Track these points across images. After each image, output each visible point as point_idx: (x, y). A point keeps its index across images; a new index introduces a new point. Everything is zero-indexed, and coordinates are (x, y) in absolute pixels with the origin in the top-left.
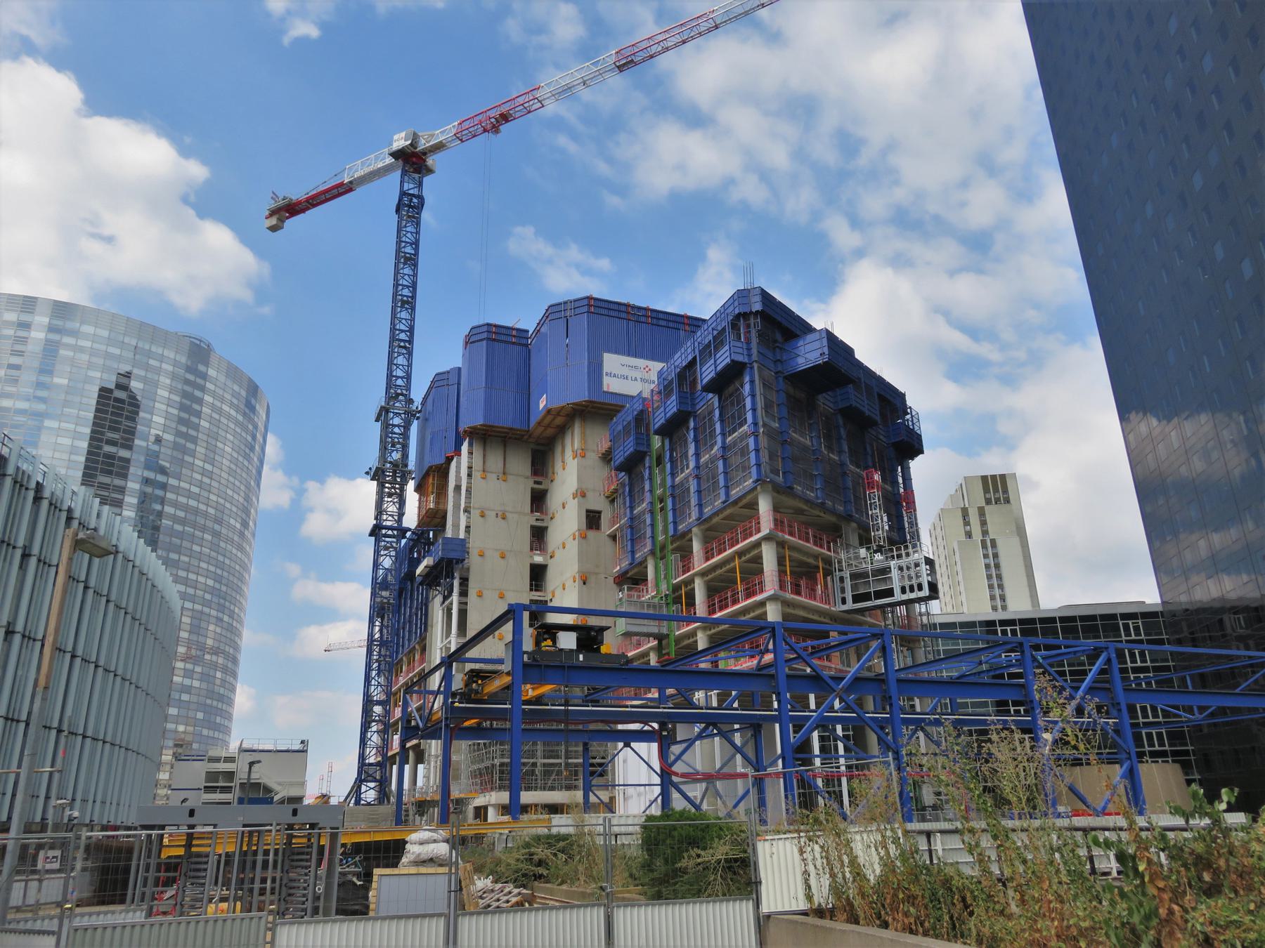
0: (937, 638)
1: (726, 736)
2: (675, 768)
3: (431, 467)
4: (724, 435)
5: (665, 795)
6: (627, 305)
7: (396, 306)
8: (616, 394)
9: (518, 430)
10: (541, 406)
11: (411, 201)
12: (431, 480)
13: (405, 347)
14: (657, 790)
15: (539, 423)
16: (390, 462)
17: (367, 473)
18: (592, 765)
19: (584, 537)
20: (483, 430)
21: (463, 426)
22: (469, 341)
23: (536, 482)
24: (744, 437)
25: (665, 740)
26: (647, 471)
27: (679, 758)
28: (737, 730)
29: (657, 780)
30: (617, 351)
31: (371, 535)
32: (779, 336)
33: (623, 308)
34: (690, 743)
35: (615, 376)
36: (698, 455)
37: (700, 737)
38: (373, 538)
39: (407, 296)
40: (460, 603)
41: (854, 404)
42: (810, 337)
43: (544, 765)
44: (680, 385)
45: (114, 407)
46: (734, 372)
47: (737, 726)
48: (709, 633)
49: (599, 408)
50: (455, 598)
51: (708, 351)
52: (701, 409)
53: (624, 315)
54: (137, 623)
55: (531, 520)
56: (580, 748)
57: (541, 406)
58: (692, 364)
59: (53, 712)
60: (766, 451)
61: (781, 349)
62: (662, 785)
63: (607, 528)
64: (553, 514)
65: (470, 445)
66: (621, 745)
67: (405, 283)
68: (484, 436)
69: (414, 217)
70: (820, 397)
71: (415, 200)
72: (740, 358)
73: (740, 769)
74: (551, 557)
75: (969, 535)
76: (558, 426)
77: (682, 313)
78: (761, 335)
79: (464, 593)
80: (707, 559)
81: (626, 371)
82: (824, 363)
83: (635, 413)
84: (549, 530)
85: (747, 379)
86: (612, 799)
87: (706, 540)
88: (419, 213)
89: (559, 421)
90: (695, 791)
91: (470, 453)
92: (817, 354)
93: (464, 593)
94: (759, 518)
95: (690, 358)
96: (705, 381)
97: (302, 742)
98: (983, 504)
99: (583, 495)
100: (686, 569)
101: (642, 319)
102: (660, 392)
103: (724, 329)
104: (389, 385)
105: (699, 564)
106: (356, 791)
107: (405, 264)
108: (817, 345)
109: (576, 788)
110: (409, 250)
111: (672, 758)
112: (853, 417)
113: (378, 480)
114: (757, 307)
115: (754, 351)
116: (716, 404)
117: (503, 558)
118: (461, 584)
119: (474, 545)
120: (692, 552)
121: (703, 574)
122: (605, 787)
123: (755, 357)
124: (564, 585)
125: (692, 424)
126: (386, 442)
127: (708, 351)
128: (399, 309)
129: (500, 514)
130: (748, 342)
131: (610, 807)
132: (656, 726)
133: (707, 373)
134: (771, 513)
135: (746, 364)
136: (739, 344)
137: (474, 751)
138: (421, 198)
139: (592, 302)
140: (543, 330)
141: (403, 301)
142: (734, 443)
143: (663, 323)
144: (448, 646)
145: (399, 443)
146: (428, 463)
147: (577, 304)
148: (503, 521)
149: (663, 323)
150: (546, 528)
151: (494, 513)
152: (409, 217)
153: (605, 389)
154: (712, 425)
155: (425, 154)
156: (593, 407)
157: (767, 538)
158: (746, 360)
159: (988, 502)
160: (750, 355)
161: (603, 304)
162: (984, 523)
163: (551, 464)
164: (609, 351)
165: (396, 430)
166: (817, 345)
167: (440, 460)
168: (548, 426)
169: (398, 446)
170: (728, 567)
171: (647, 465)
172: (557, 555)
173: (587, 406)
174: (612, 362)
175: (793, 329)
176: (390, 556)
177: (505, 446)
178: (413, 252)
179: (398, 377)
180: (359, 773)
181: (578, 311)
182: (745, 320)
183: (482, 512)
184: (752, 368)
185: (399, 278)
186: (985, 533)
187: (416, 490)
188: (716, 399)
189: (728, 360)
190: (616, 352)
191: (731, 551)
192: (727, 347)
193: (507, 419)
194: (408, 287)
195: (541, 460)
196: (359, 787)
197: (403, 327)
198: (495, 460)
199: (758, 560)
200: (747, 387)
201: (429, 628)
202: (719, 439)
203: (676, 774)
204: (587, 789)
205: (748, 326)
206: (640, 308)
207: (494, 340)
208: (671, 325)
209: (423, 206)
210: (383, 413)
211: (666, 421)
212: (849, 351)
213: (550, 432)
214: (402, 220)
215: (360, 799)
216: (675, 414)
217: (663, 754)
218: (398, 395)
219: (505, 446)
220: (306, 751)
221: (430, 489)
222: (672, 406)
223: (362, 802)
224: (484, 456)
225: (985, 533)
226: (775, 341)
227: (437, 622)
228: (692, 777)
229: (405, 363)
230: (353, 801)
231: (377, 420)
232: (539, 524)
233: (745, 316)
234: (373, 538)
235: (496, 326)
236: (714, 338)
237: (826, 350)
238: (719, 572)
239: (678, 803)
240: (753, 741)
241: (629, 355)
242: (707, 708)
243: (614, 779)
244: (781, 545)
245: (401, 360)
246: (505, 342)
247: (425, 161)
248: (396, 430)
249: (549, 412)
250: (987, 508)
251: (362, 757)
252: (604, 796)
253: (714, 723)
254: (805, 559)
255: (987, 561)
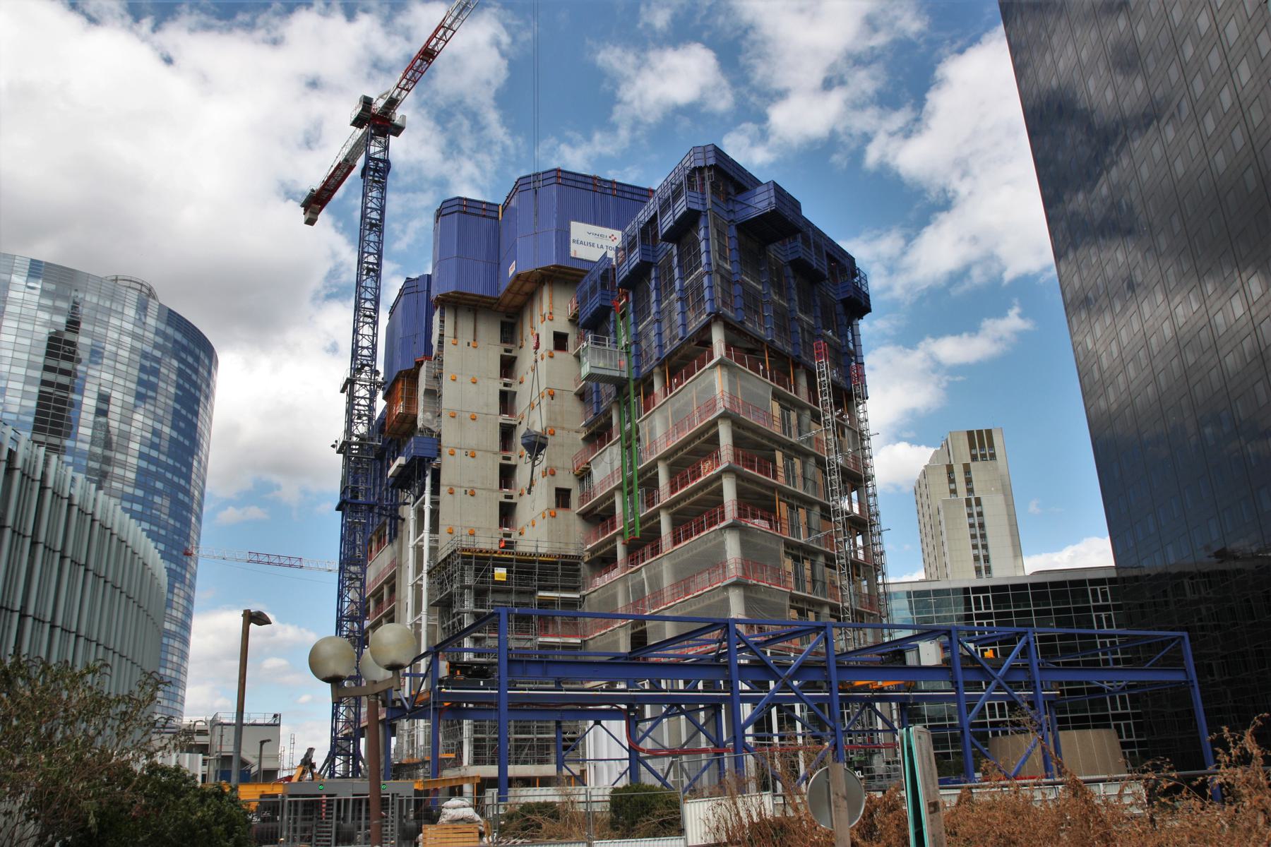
0: (882, 628)
1: (691, 717)
2: (641, 745)
3: (400, 372)
4: (682, 279)
5: (633, 771)
6: (594, 178)
7: (362, 274)
8: (582, 260)
9: (488, 298)
10: (511, 273)
11: (377, 164)
12: (400, 386)
13: (370, 316)
14: (627, 763)
15: (509, 290)
16: (357, 436)
17: (333, 446)
18: (564, 740)
19: (551, 357)
20: (454, 297)
21: (435, 294)
22: (440, 214)
23: (505, 458)
24: (701, 276)
25: (633, 719)
26: (612, 325)
27: (646, 734)
28: (702, 709)
29: (626, 755)
30: (583, 221)
31: (338, 509)
32: (731, 190)
33: (590, 181)
34: (657, 720)
35: (581, 243)
36: (659, 302)
37: (666, 715)
38: (340, 512)
39: (376, 220)
40: (432, 503)
41: (803, 257)
42: (759, 190)
43: (516, 740)
44: (643, 240)
45: (54, 408)
46: (690, 221)
47: (701, 706)
48: (674, 562)
49: (564, 273)
50: (427, 495)
51: (666, 206)
52: (661, 259)
53: (590, 187)
54: (131, 601)
55: (499, 460)
56: (552, 724)
57: (511, 273)
58: (654, 219)
59: (14, 597)
60: (719, 289)
61: (733, 201)
62: (630, 759)
63: (576, 506)
64: (523, 529)
65: (442, 315)
66: (591, 723)
67: (373, 206)
68: (457, 303)
69: (379, 182)
70: (772, 247)
71: (381, 165)
72: (696, 207)
73: (703, 746)
74: (520, 534)
75: (953, 492)
76: (527, 294)
77: (647, 187)
78: (714, 186)
79: (436, 490)
80: (672, 493)
81: (591, 239)
82: (772, 211)
83: (601, 272)
84: (519, 507)
85: (702, 225)
86: (583, 772)
87: (672, 475)
88: (384, 178)
89: (528, 287)
90: (660, 765)
91: (442, 321)
92: (766, 203)
93: (436, 490)
94: (723, 507)
95: (652, 213)
96: (664, 231)
97: (275, 716)
98: (968, 460)
99: (553, 474)
100: (650, 503)
101: (609, 191)
102: (624, 249)
103: (681, 183)
104: (355, 355)
105: (665, 494)
106: (329, 766)
107: (370, 229)
108: (765, 196)
109: (546, 762)
110: (375, 215)
111: (641, 734)
112: (800, 267)
113: (344, 454)
114: (711, 162)
115: (709, 201)
116: (675, 252)
117: (474, 383)
118: (433, 479)
119: (447, 440)
120: (660, 537)
121: (667, 507)
122: (577, 761)
123: (709, 205)
124: (533, 521)
125: (653, 275)
126: (352, 414)
127: (666, 206)
128: (365, 277)
129: (469, 490)
130: (703, 193)
131: (581, 779)
132: (624, 707)
133: (667, 223)
134: (731, 448)
135: (700, 212)
136: (695, 195)
137: (448, 726)
138: (387, 162)
139: (560, 174)
140: (513, 203)
141: (368, 268)
142: (691, 285)
143: (627, 195)
144: (420, 543)
145: (365, 415)
146: (399, 367)
147: (546, 176)
148: (472, 460)
149: (627, 195)
150: (515, 358)
151: (463, 490)
152: (375, 182)
153: (572, 255)
154: (671, 270)
155: (386, 113)
156: (560, 273)
157: (727, 471)
158: (700, 208)
159: (974, 458)
160: (704, 205)
161: (570, 176)
162: (969, 481)
163: (519, 332)
164: (576, 220)
165: (362, 402)
166: (765, 196)
167: (412, 366)
168: (517, 293)
169: (365, 418)
170: (692, 499)
171: (612, 319)
172: (527, 531)
173: (555, 271)
174: (579, 230)
175: (745, 184)
176: (355, 588)
177: (475, 314)
178: (378, 217)
179: (366, 300)
180: (332, 747)
181: (546, 182)
182: (700, 174)
183: (451, 489)
184: (706, 215)
185: (365, 244)
186: (970, 491)
187: (384, 398)
188: (675, 247)
189: (685, 209)
190: (583, 221)
191: (694, 484)
192: (684, 198)
193: (477, 288)
194: (376, 210)
195: (510, 332)
196: (334, 761)
197: (371, 250)
198: (466, 326)
199: (719, 492)
200: (702, 233)
201: (399, 534)
202: (677, 284)
203: (643, 751)
204: (560, 766)
205: (703, 179)
206: (606, 181)
207: (465, 212)
208: (636, 197)
209: (389, 170)
210: (349, 384)
211: (630, 272)
212: (796, 205)
213: (519, 299)
214: (365, 229)
215: (335, 772)
216: (638, 264)
217: (630, 733)
218: (363, 366)
219: (475, 314)
220: (278, 725)
221: (400, 394)
222: (636, 258)
223: (337, 775)
224: (456, 323)
225: (970, 491)
226: (729, 194)
227: (407, 596)
228: (654, 754)
229: (376, 239)
230: (327, 775)
231: (342, 391)
232: (507, 380)
233: (699, 170)
234: (340, 512)
235: (466, 199)
236: (673, 193)
237: (773, 200)
238: (683, 504)
239: (647, 779)
240: (714, 719)
241: (595, 224)
242: (671, 691)
243: (584, 753)
244: (740, 477)
245: (366, 330)
246: (478, 215)
247: (390, 120)
248: (362, 402)
249: (518, 277)
250: (973, 465)
251: (334, 730)
252: (576, 769)
253: (675, 705)
254: (763, 491)
255: (971, 521)
